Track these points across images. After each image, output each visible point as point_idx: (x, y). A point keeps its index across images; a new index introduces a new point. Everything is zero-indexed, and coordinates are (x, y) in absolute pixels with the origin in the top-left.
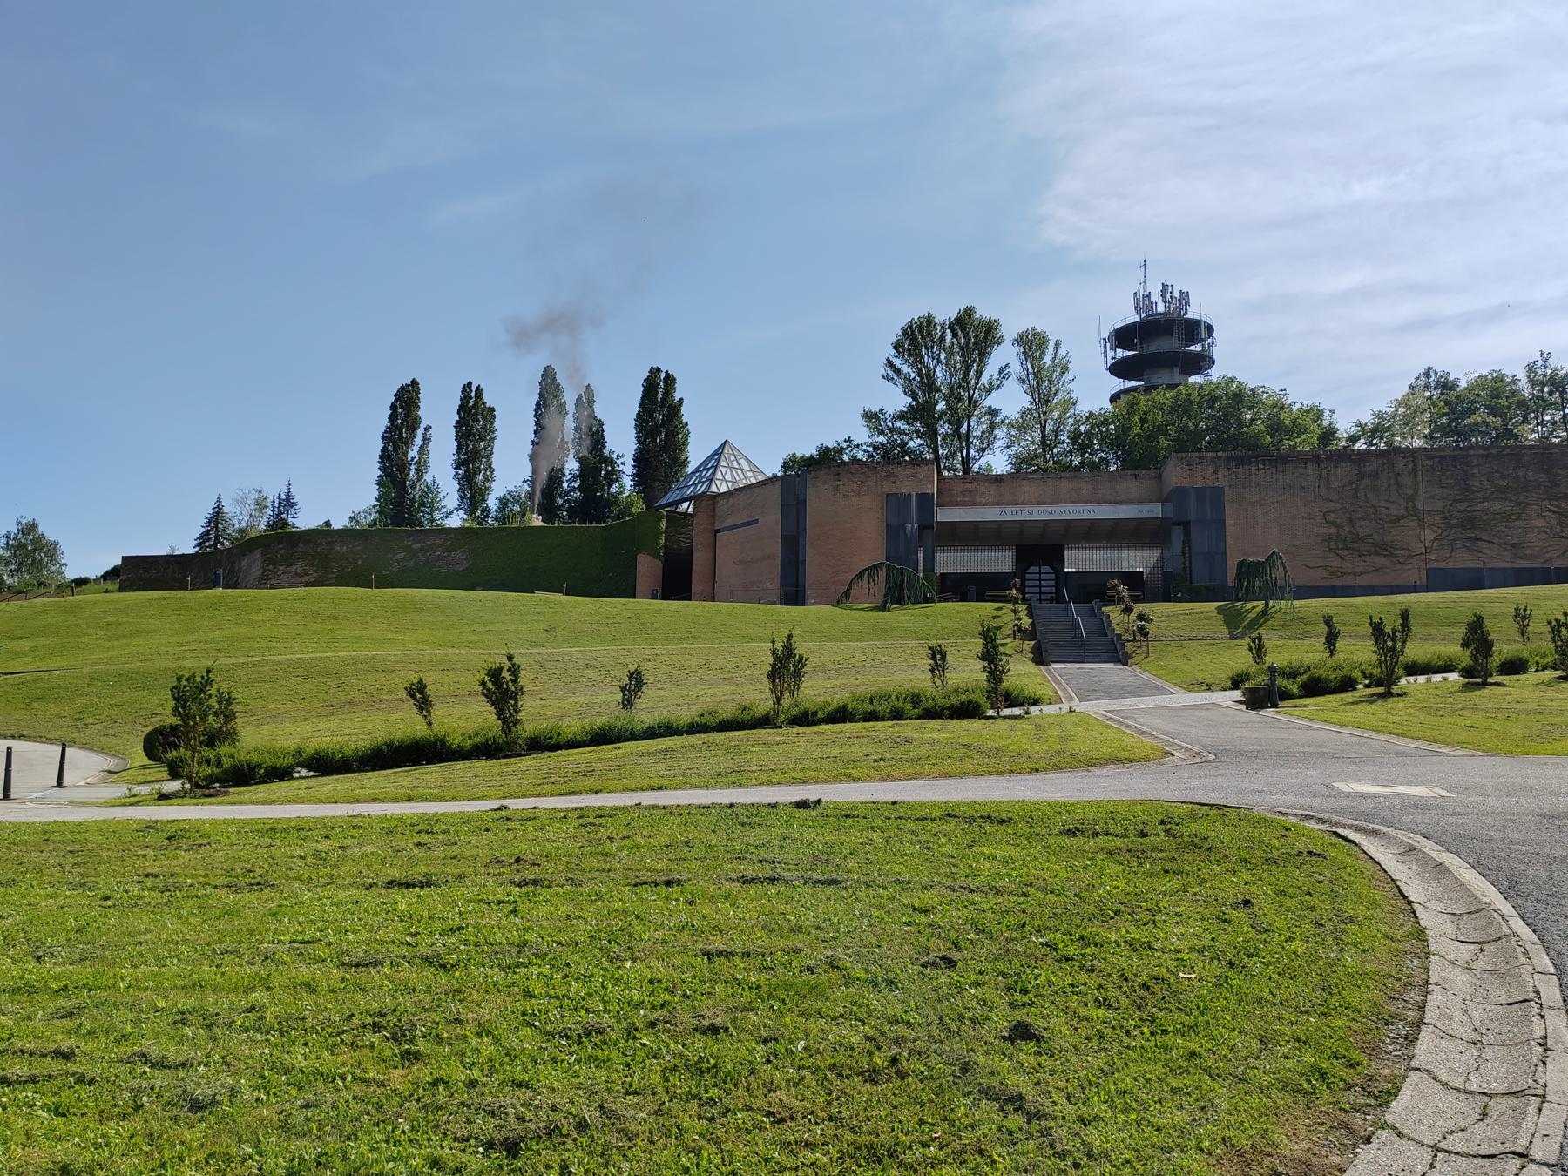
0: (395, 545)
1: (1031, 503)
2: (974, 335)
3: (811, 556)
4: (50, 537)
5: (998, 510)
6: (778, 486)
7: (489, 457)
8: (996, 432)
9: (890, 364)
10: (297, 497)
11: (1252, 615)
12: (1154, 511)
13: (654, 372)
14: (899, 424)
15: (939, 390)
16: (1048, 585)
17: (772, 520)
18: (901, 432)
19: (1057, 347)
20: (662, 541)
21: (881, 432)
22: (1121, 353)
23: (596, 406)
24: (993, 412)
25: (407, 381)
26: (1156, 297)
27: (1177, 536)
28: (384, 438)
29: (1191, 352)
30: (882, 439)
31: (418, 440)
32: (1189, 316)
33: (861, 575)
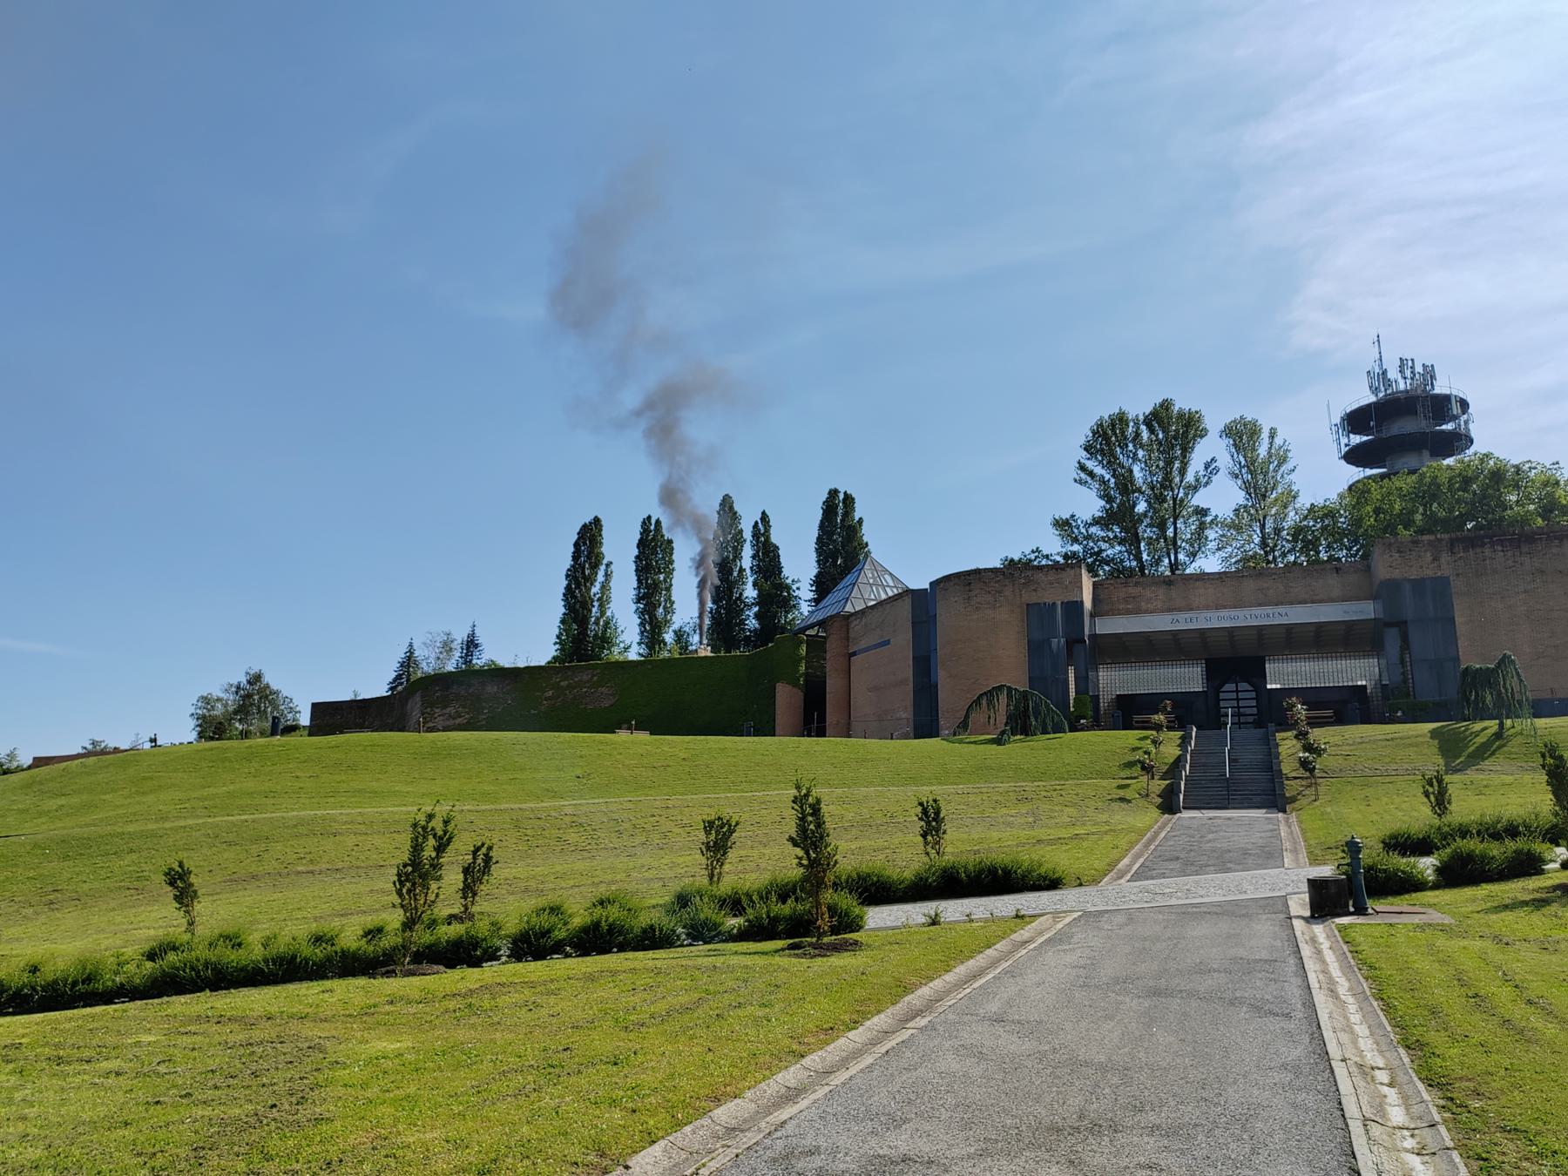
0: (582, 688)
1: (1207, 608)
2: (1174, 430)
3: (943, 679)
4: (274, 687)
5: (1167, 617)
6: (908, 601)
7: (668, 589)
8: (1208, 532)
9: (1082, 468)
10: (481, 638)
11: (1480, 740)
12: (1365, 610)
13: (833, 493)
14: (1093, 530)
15: (1139, 490)
16: (1250, 705)
17: (903, 640)
18: (1096, 540)
19: (1272, 436)
20: (802, 668)
21: (1075, 540)
22: (1356, 439)
23: (772, 531)
24: (1202, 512)
25: (588, 519)
26: (1393, 374)
27: (1392, 638)
28: (567, 576)
29: (1443, 432)
30: (1076, 548)
31: (600, 577)
32: (1437, 391)
33: (978, 701)
